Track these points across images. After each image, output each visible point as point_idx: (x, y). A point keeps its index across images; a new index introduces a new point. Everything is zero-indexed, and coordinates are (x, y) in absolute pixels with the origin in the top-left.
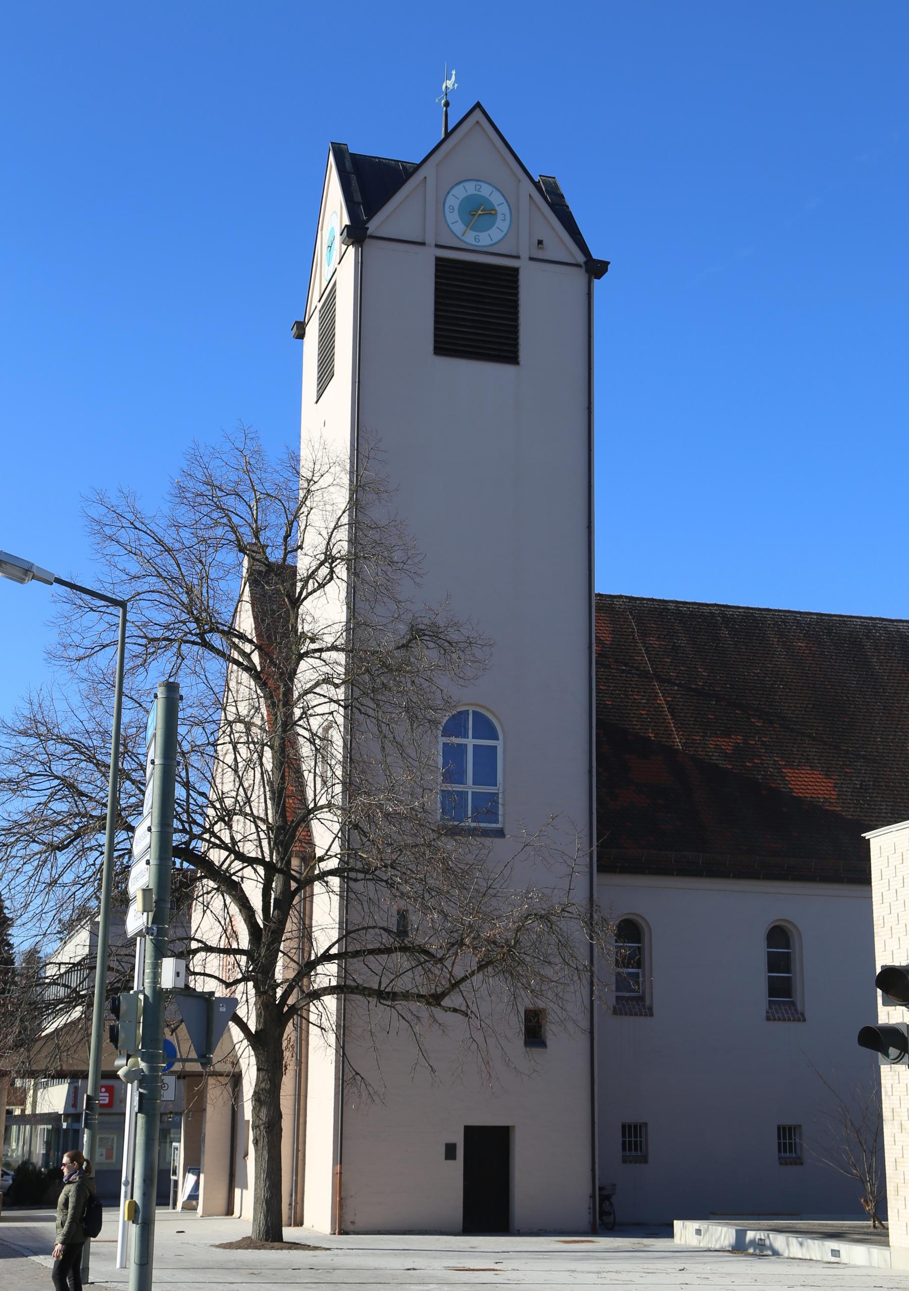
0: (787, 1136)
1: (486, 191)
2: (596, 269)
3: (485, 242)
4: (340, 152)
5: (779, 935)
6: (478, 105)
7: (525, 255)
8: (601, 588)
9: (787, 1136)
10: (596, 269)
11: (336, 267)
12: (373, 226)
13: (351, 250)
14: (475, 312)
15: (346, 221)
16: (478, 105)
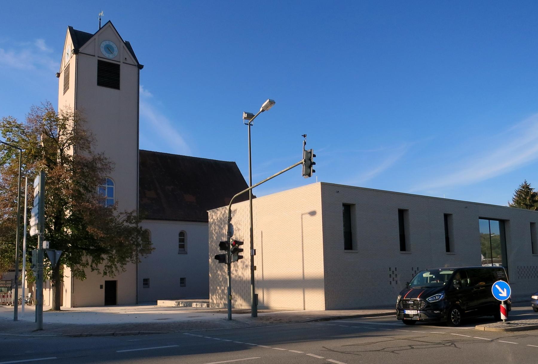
0: (183, 280)
1: (111, 44)
2: (140, 67)
3: (109, 57)
4: (71, 29)
5: (182, 234)
6: (110, 21)
7: (122, 62)
8: (140, 148)
9: (183, 280)
10: (140, 67)
11: (69, 59)
12: (81, 50)
13: (75, 55)
14: (108, 75)
15: (73, 48)
16: (110, 21)
